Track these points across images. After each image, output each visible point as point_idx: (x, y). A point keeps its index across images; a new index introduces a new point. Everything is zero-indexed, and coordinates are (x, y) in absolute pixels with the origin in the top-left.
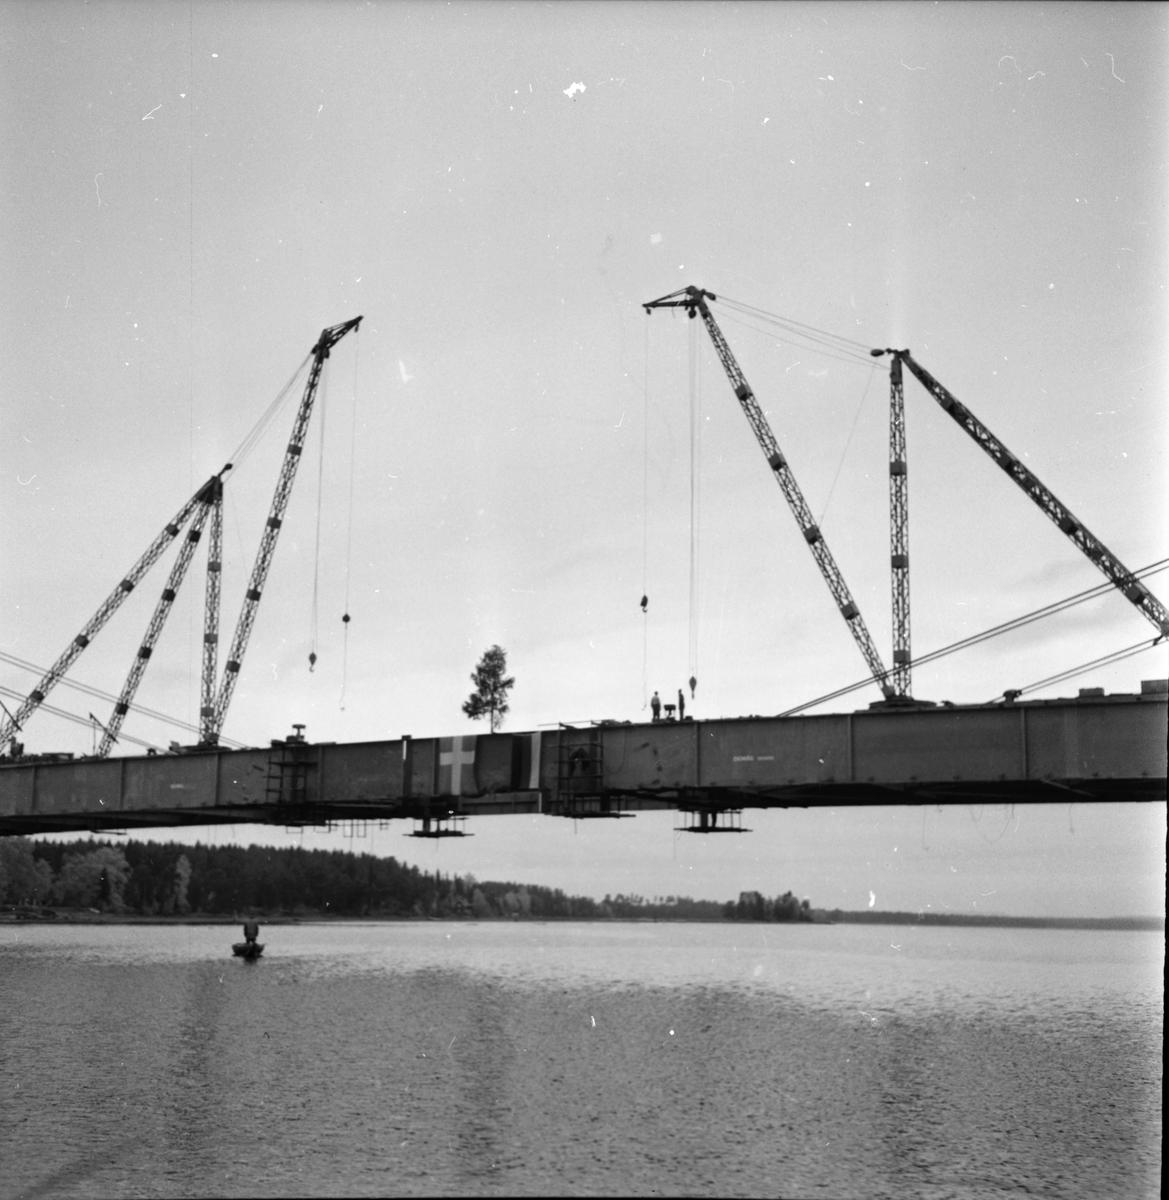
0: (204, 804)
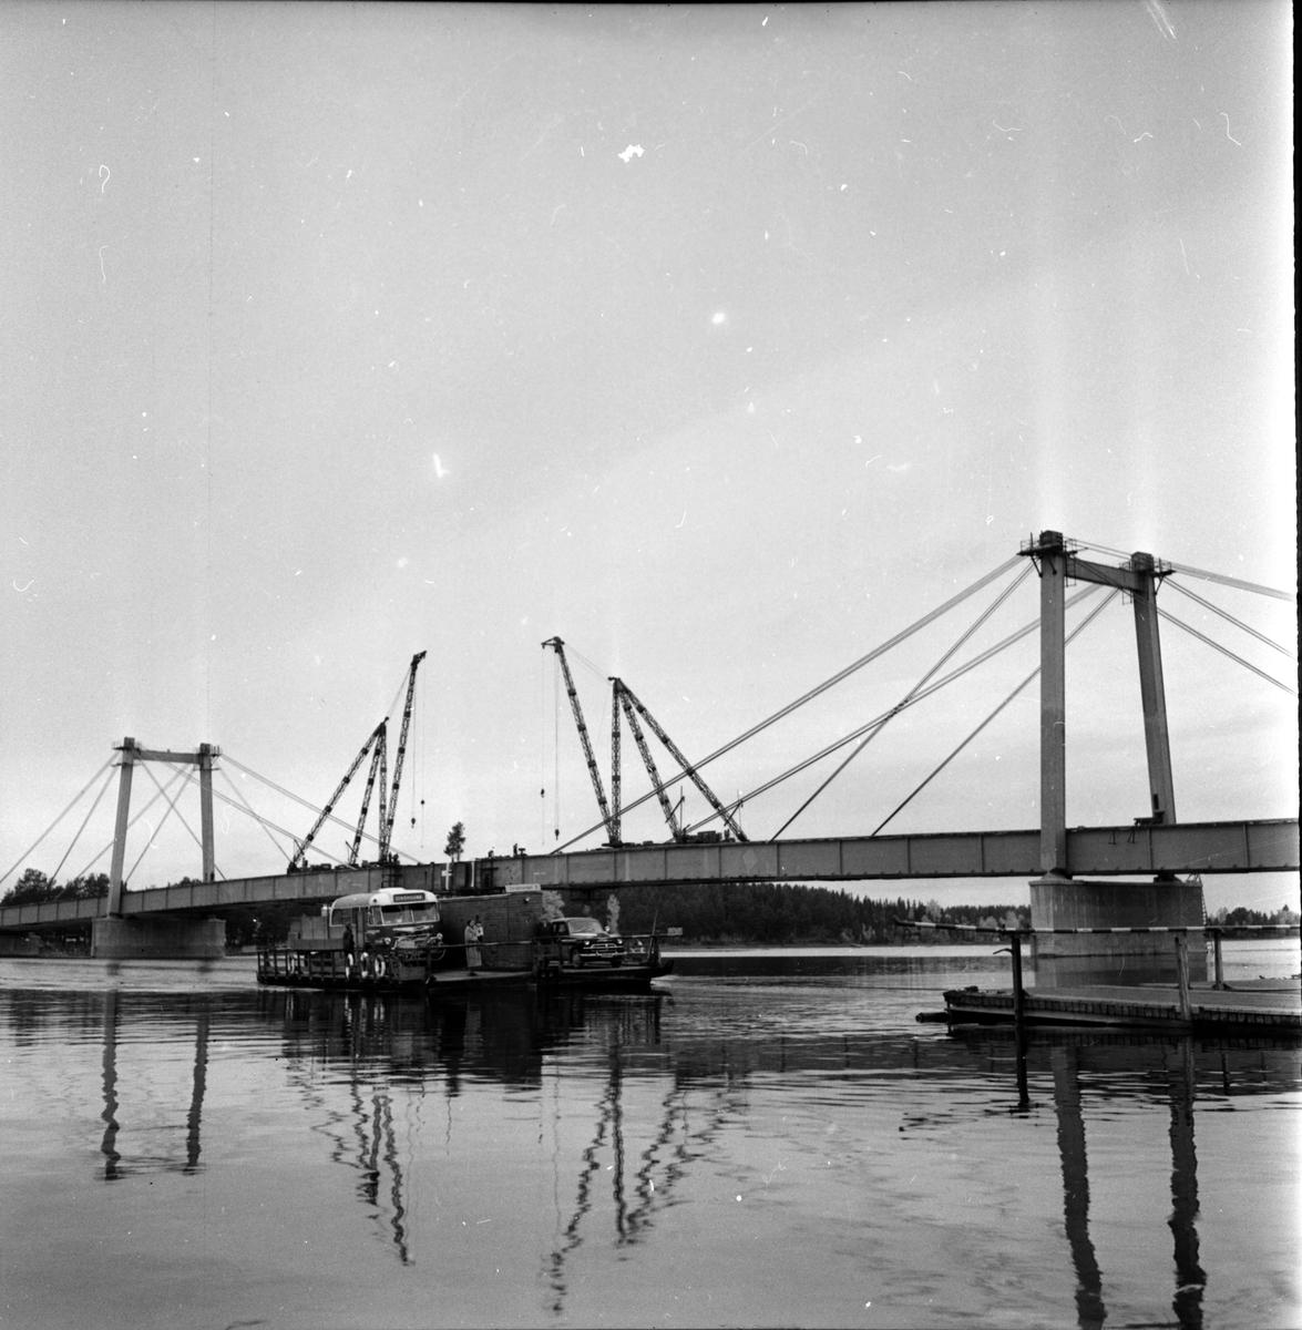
0: (1235, 866)
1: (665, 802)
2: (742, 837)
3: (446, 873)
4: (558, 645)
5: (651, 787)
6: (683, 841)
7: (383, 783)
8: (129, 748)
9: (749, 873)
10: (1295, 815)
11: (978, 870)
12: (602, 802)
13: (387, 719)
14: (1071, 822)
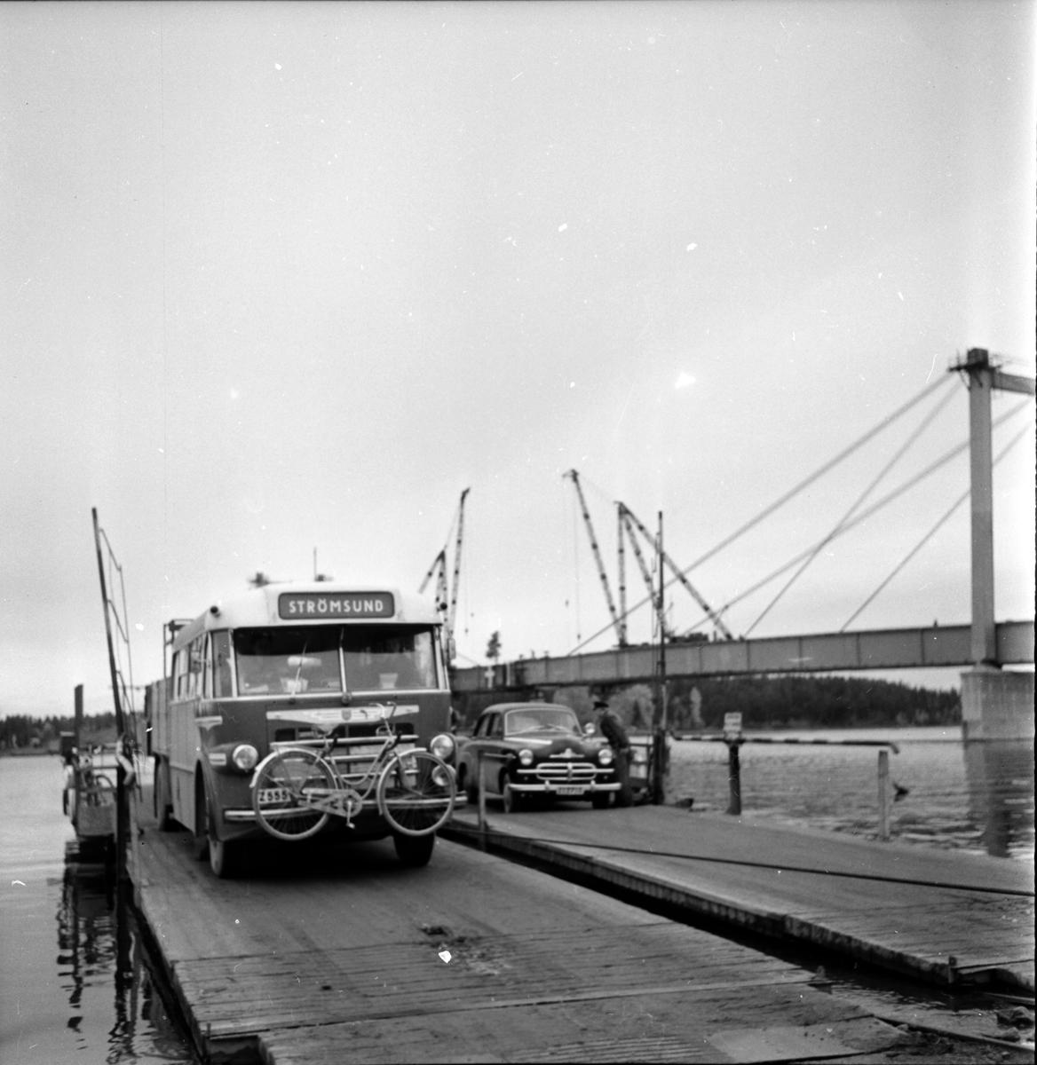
2: (729, 636)
3: (490, 674)
4: (575, 476)
10: (1033, 618)
11: (919, 661)
12: (612, 609)
13: (446, 547)
14: (1000, 616)
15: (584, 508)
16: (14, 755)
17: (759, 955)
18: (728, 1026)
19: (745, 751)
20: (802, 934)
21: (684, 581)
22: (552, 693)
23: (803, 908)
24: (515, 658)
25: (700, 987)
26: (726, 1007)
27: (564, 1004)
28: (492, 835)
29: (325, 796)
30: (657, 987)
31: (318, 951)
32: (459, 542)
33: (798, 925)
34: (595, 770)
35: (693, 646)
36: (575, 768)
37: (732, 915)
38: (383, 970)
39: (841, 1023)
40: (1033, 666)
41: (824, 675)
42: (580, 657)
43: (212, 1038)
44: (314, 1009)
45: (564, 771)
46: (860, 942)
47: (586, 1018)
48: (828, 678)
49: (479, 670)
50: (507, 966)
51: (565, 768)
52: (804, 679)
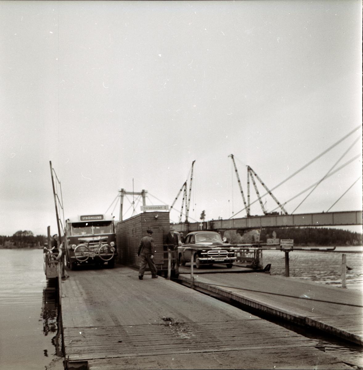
1: (261, 203)
2: (286, 213)
4: (232, 157)
5: (257, 198)
6: (267, 215)
7: (186, 199)
8: (122, 191)
9: (285, 224)
10: (362, 210)
12: (245, 203)
13: (187, 180)
15: (236, 168)
16: (39, 248)
17: (295, 334)
18: (282, 365)
19: (291, 254)
20: (312, 325)
21: (271, 194)
22: (224, 232)
23: (314, 315)
24: (210, 219)
25: (271, 347)
26: (281, 356)
27: (214, 353)
28: (195, 282)
29: (88, 254)
30: (253, 346)
31: (120, 326)
32: (191, 179)
33: (311, 321)
34: (227, 253)
35: (273, 217)
36: (221, 252)
37: (285, 316)
38: (144, 335)
39: (329, 365)
40: (362, 247)
41: (321, 227)
42: (233, 219)
43: (69, 362)
44: (113, 350)
45: (217, 253)
46: (336, 329)
47: (222, 359)
48: (322, 228)
49: (198, 223)
50: (193, 335)
51: (218, 252)
52: (313, 228)
